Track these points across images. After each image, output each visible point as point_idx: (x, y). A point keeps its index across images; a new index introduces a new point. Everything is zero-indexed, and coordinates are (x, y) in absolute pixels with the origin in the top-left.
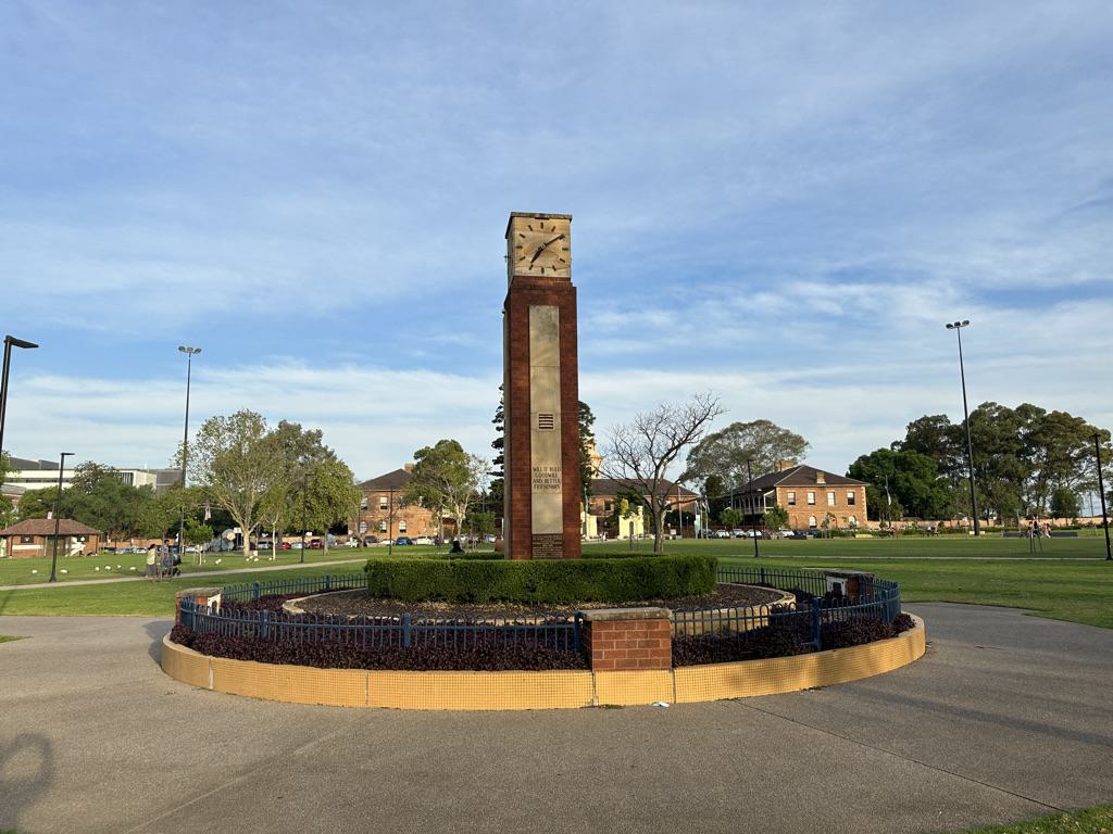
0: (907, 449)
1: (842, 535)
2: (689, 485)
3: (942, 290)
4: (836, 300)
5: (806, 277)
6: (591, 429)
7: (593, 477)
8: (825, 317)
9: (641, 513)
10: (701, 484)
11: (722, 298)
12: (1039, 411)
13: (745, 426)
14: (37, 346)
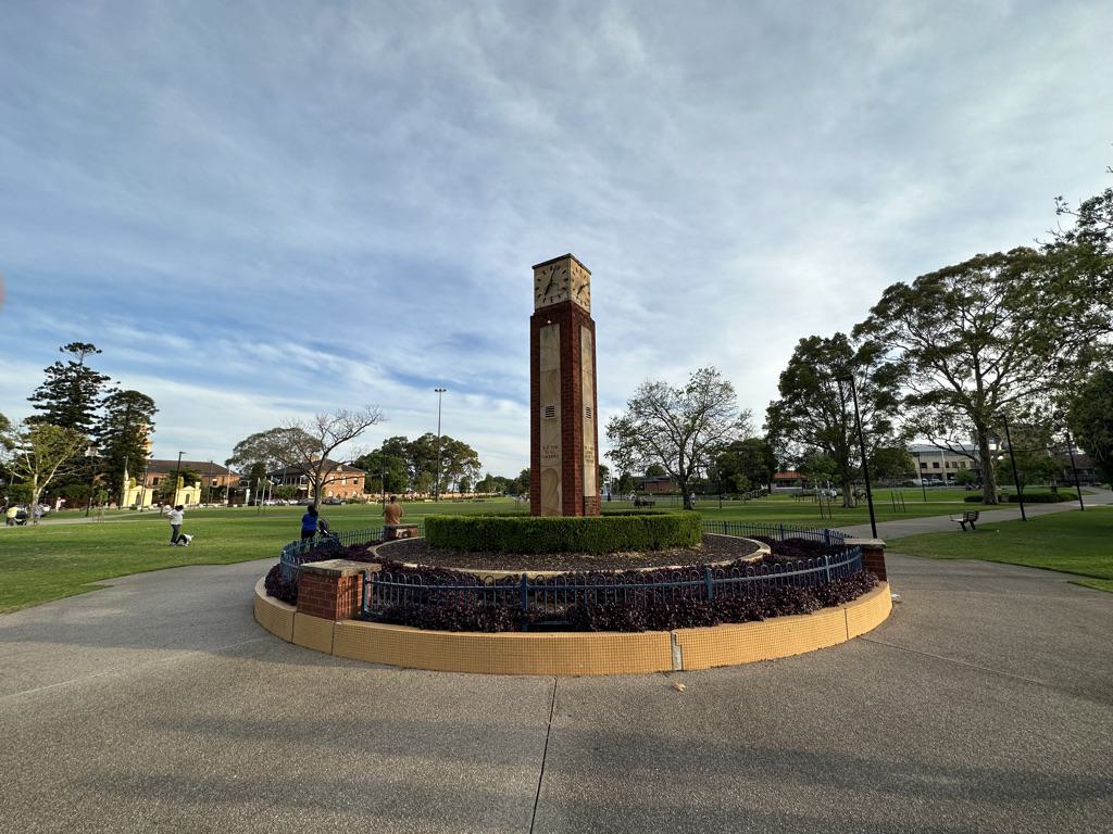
0: (389, 453)
1: (358, 502)
2: (232, 468)
3: (376, 368)
4: (315, 360)
5: (297, 342)
6: (152, 419)
7: (148, 458)
8: (306, 369)
9: (197, 488)
10: (241, 468)
11: (233, 340)
12: (451, 440)
13: (283, 431)
14: (555, 275)
